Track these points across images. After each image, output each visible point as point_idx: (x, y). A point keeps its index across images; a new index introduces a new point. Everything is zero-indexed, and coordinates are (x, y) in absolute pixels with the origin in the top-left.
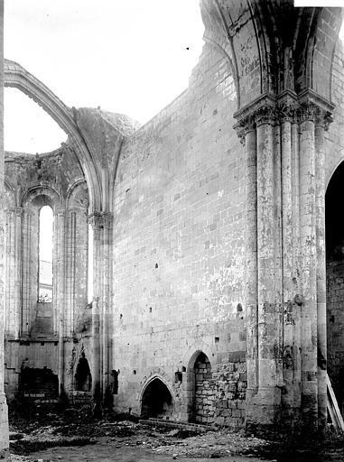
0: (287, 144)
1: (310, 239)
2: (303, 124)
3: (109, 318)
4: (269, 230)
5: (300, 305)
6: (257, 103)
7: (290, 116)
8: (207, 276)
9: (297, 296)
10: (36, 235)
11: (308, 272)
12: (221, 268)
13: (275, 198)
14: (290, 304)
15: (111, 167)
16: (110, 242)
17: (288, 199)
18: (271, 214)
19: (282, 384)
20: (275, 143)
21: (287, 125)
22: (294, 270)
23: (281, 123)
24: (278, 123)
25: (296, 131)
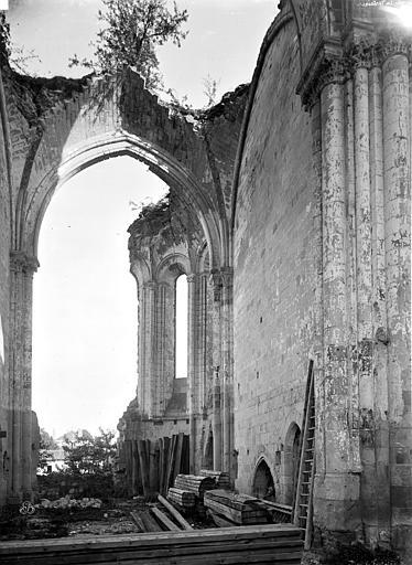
0: (363, 102)
1: (398, 237)
2: (386, 64)
3: (229, 388)
4: (335, 237)
5: (386, 343)
6: (315, 59)
7: (363, 59)
8: (299, 323)
9: (380, 330)
10: (171, 307)
11: (396, 290)
12: (310, 309)
13: (346, 188)
14: (369, 344)
15: (229, 213)
16: (230, 302)
17: (364, 184)
18: (338, 213)
19: (359, 468)
20: (345, 107)
21: (362, 74)
22: (375, 291)
23: (353, 78)
24: (349, 76)
25: (375, 78)
